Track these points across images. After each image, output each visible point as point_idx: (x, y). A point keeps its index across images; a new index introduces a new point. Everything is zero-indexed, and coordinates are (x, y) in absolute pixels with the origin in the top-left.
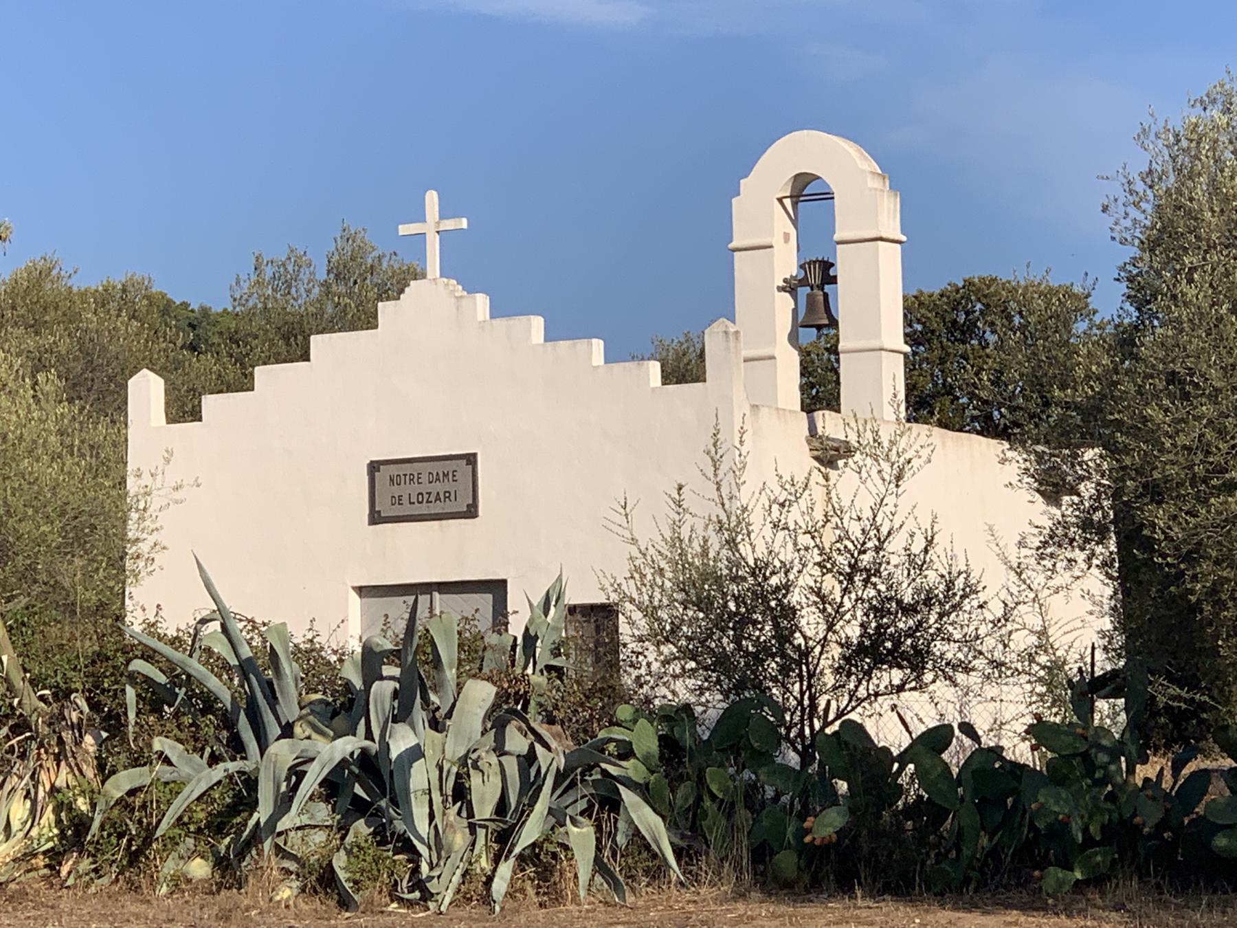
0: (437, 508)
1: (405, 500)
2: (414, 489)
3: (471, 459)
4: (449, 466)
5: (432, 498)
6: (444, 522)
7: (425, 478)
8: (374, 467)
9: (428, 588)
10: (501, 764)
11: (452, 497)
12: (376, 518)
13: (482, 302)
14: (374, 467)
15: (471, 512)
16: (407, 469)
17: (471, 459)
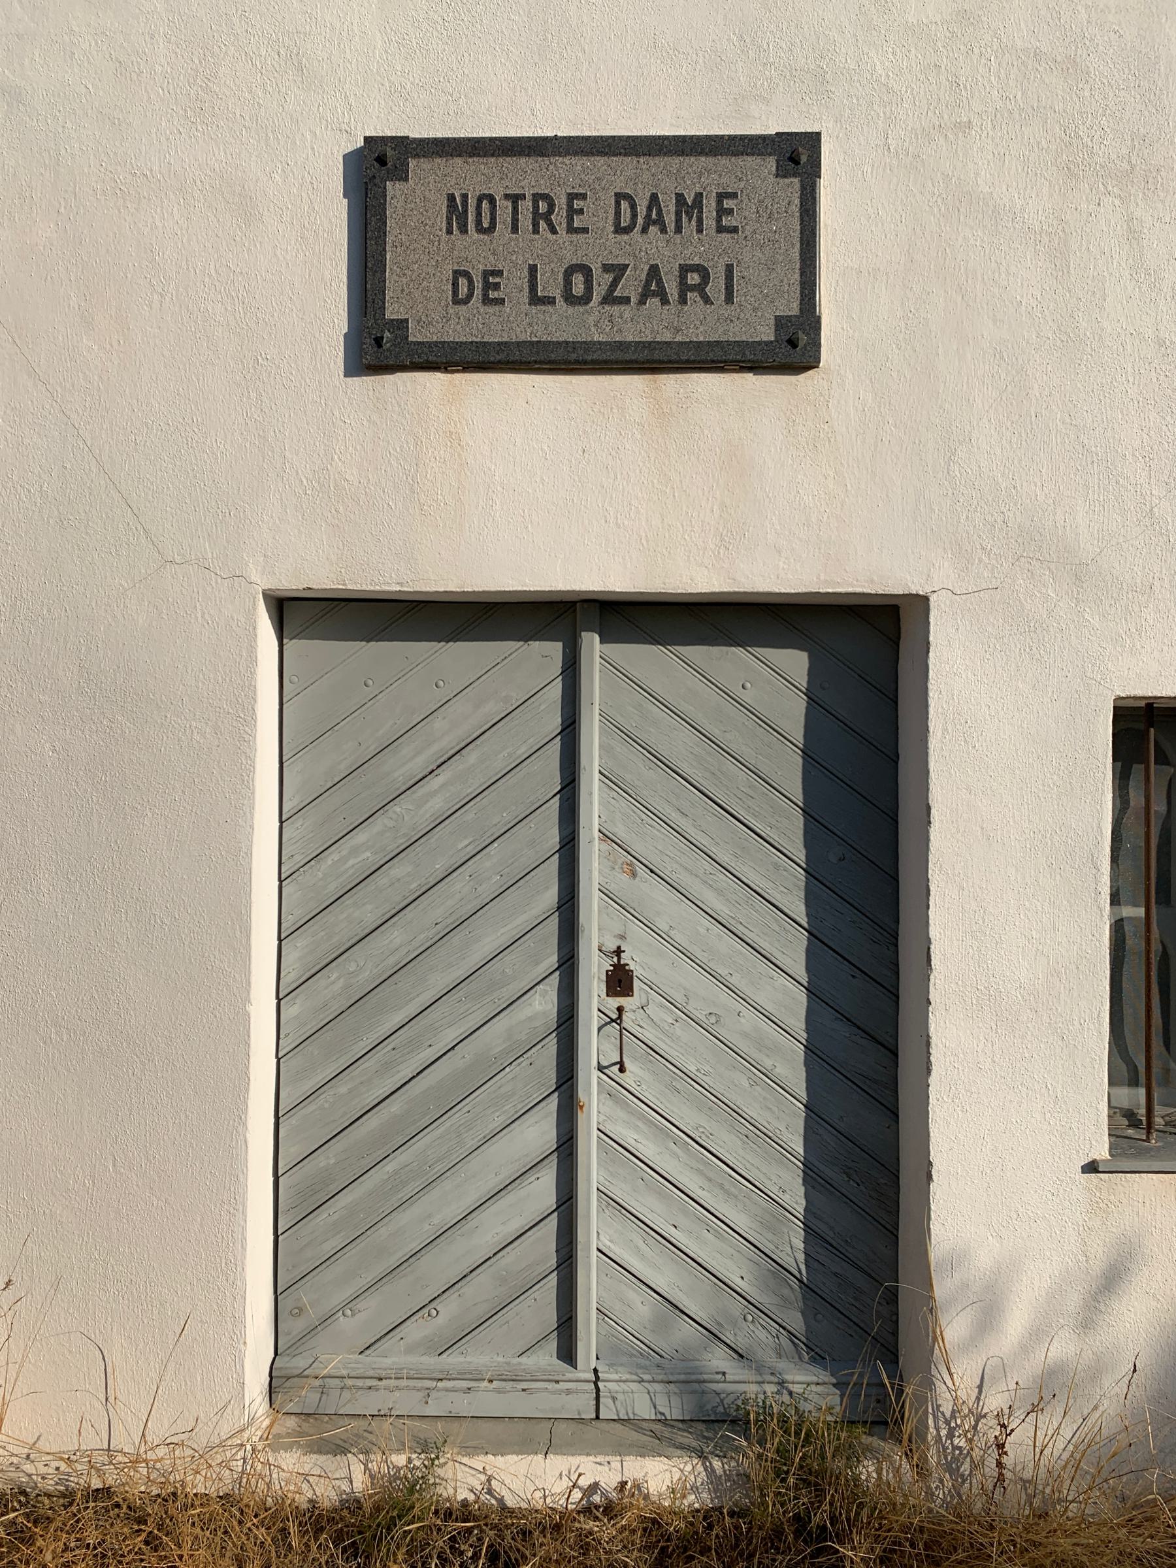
1: (514, 285)
2: (555, 251)
3: (797, 155)
5: (629, 287)
6: (670, 383)
7: (598, 214)
8: (377, 167)
11: (715, 288)
12: (379, 346)
15: (792, 348)
16: (527, 176)
17: (797, 155)
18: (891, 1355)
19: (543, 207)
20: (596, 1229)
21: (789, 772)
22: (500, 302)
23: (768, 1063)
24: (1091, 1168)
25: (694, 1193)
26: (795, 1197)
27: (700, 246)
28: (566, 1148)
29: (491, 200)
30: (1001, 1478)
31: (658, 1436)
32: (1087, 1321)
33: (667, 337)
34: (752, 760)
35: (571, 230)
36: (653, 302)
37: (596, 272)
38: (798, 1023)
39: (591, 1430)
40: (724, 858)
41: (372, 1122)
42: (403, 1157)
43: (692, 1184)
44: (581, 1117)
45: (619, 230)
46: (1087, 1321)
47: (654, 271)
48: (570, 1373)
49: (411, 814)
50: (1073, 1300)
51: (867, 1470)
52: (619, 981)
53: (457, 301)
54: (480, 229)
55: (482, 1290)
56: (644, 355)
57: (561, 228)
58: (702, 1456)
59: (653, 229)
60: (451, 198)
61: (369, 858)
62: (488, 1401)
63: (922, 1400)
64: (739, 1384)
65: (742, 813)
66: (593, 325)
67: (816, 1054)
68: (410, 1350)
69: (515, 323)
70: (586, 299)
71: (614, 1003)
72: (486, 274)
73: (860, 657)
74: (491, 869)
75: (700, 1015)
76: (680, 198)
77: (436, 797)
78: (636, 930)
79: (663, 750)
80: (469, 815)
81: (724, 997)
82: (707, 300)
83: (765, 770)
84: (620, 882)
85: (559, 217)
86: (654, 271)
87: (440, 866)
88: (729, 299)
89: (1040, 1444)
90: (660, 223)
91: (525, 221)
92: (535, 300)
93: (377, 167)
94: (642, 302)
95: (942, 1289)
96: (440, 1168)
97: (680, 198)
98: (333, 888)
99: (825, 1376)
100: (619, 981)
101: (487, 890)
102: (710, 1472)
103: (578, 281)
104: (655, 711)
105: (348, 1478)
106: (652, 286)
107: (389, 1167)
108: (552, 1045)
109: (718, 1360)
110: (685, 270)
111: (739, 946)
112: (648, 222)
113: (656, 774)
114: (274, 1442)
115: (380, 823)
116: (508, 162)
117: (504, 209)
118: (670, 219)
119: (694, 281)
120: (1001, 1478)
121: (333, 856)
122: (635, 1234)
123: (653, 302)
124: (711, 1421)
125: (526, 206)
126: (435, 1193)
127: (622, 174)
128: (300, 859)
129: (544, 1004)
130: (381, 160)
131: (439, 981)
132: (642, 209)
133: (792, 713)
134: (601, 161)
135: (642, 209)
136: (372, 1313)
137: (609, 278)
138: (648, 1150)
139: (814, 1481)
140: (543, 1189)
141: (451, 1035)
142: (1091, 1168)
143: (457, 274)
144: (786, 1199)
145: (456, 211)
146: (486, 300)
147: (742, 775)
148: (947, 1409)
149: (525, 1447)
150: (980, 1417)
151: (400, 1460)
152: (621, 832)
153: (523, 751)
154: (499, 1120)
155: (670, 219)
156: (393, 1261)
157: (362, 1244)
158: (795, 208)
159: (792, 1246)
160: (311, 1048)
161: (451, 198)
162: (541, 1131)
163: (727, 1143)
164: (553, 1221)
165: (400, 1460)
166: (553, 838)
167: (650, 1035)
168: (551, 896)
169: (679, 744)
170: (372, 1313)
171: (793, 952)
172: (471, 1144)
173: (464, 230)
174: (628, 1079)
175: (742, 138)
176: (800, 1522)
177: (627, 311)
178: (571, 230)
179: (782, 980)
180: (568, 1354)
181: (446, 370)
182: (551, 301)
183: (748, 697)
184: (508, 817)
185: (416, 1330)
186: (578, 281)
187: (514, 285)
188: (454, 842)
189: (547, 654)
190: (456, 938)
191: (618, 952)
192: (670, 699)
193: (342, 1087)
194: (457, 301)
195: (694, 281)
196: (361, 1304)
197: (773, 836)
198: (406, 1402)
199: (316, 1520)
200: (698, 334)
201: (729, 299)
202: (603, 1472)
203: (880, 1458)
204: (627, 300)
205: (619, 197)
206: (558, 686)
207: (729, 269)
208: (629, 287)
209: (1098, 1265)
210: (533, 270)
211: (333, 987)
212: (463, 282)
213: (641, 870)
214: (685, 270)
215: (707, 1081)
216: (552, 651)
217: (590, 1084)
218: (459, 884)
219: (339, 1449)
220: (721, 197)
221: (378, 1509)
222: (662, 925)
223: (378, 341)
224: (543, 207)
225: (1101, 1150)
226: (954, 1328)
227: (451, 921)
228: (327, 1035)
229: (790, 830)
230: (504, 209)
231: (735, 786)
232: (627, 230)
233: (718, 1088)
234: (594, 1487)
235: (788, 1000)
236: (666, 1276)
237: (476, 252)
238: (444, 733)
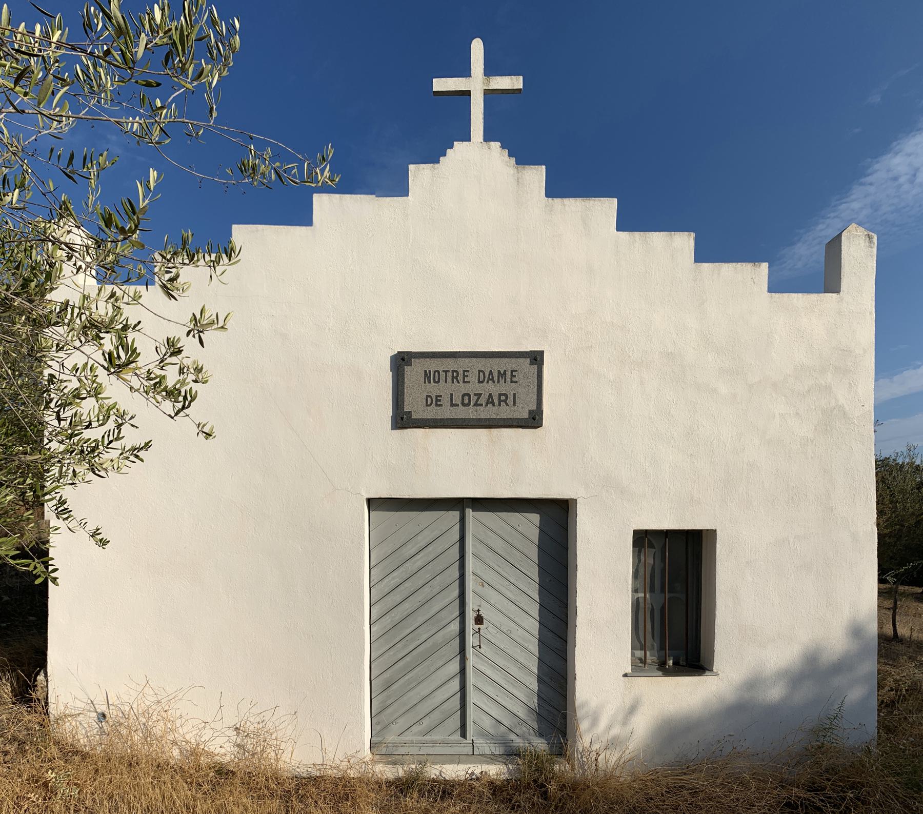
0: (485, 413)
1: (446, 400)
2: (459, 389)
3: (536, 358)
4: (506, 365)
5: (483, 401)
6: (495, 431)
7: (473, 377)
8: (401, 361)
9: (459, 504)
10: (200, 337)
11: (510, 401)
12: (402, 420)
13: (537, 176)
14: (401, 362)
15: (534, 420)
16: (450, 364)
17: (536, 358)
18: (564, 734)
19: (455, 374)
20: (472, 697)
21: (534, 552)
22: (441, 405)
23: (526, 645)
24: (625, 675)
25: (504, 685)
26: (535, 686)
27: (505, 387)
28: (463, 671)
29: (439, 372)
30: (597, 770)
31: (492, 759)
32: (625, 722)
33: (494, 417)
34: (521, 549)
35: (464, 382)
36: (490, 405)
37: (472, 396)
38: (536, 633)
39: (472, 757)
40: (512, 581)
41: (401, 664)
42: (410, 675)
43: (503, 683)
44: (467, 662)
45: (479, 382)
46: (625, 722)
47: (490, 395)
48: (465, 741)
49: (411, 566)
50: (620, 717)
51: (557, 767)
52: (479, 620)
53: (427, 405)
54: (435, 382)
55: (436, 716)
56: (487, 423)
57: (461, 382)
58: (506, 764)
59: (490, 382)
60: (426, 371)
61: (398, 581)
62: (438, 750)
63: (572, 746)
64: (518, 742)
65: (518, 566)
66: (470, 413)
67: (541, 642)
68: (415, 734)
69: (446, 412)
70: (469, 404)
71: (477, 627)
72: (437, 396)
73: (556, 516)
74: (437, 583)
75: (505, 631)
76: (499, 371)
77: (419, 561)
78: (484, 603)
79: (492, 546)
80: (430, 567)
81: (513, 625)
82: (507, 405)
83: (526, 552)
84: (479, 589)
85: (460, 378)
86: (490, 395)
87: (421, 583)
88: (514, 404)
89: (610, 759)
90: (493, 380)
91: (449, 379)
92: (452, 405)
93: (401, 361)
94: (486, 405)
95: (580, 713)
96: (422, 678)
97: (499, 371)
98: (387, 590)
99: (544, 741)
100: (479, 620)
101: (435, 591)
102: (508, 768)
103: (466, 398)
104: (490, 533)
105: (400, 772)
106: (490, 400)
107: (406, 678)
108: (457, 640)
109: (513, 737)
110: (500, 395)
111: (517, 608)
112: (489, 379)
113: (491, 554)
114: (374, 762)
115: (401, 569)
116: (444, 360)
117: (443, 374)
118: (496, 378)
119: (503, 398)
120: (597, 770)
121: (386, 580)
122: (485, 698)
123: (490, 405)
124: (511, 754)
125: (450, 374)
126: (421, 686)
127: (480, 364)
128: (376, 581)
129: (455, 627)
130: (403, 359)
131: (421, 620)
132: (487, 375)
133: (534, 534)
134: (474, 359)
135: (487, 375)
136: (402, 723)
137: (476, 398)
138: (488, 672)
139: (539, 770)
140: (455, 685)
141: (425, 637)
142: (625, 675)
143: (427, 396)
144: (532, 687)
145: (427, 376)
146: (437, 405)
147: (518, 554)
148: (581, 749)
149: (451, 762)
150: (591, 752)
151: (413, 766)
152: (479, 572)
153: (447, 547)
154: (441, 663)
155: (496, 378)
156: (408, 707)
157: (399, 702)
158: (535, 375)
159: (534, 702)
160: (381, 640)
161: (426, 371)
162: (455, 667)
163: (514, 670)
164: (459, 694)
165: (413, 766)
166: (457, 574)
167: (489, 637)
168: (456, 593)
169: (498, 544)
170: (402, 723)
171: (535, 610)
172: (433, 670)
173: (429, 382)
174: (482, 650)
175: (519, 352)
176: (535, 781)
177: (482, 408)
178: (464, 382)
179: (531, 619)
180: (464, 735)
181: (423, 427)
182: (457, 405)
183: (520, 529)
184: (442, 568)
185: (416, 729)
186: (466, 398)
187: (446, 400)
188: (425, 576)
189: (455, 515)
190: (426, 606)
191: (478, 611)
192: (495, 530)
193: (391, 653)
194: (427, 405)
195: (503, 398)
196: (398, 721)
197: (528, 574)
198: (414, 750)
199: (389, 784)
200: (504, 416)
201: (514, 404)
202: (477, 769)
203: (559, 763)
204: (481, 405)
205: (480, 371)
206: (458, 525)
207: (514, 395)
208: (483, 401)
209: (628, 705)
210: (452, 395)
211: (387, 621)
212: (429, 399)
213: (485, 585)
214: (500, 395)
215: (507, 651)
216: (456, 514)
217: (470, 652)
218: (426, 589)
219: (395, 763)
220: (512, 371)
221: (407, 780)
222: (492, 602)
223: (402, 418)
224: (455, 374)
225: (629, 670)
226: (584, 726)
227: (424, 601)
228: (386, 636)
229: (534, 572)
230: (443, 374)
231: (516, 557)
232: (482, 382)
233: (511, 653)
234: (473, 773)
235: (533, 626)
236: (496, 712)
237: (433, 389)
238: (422, 541)
